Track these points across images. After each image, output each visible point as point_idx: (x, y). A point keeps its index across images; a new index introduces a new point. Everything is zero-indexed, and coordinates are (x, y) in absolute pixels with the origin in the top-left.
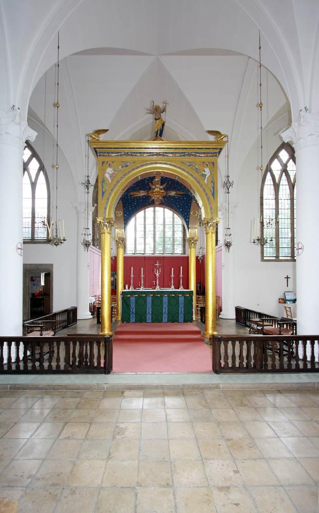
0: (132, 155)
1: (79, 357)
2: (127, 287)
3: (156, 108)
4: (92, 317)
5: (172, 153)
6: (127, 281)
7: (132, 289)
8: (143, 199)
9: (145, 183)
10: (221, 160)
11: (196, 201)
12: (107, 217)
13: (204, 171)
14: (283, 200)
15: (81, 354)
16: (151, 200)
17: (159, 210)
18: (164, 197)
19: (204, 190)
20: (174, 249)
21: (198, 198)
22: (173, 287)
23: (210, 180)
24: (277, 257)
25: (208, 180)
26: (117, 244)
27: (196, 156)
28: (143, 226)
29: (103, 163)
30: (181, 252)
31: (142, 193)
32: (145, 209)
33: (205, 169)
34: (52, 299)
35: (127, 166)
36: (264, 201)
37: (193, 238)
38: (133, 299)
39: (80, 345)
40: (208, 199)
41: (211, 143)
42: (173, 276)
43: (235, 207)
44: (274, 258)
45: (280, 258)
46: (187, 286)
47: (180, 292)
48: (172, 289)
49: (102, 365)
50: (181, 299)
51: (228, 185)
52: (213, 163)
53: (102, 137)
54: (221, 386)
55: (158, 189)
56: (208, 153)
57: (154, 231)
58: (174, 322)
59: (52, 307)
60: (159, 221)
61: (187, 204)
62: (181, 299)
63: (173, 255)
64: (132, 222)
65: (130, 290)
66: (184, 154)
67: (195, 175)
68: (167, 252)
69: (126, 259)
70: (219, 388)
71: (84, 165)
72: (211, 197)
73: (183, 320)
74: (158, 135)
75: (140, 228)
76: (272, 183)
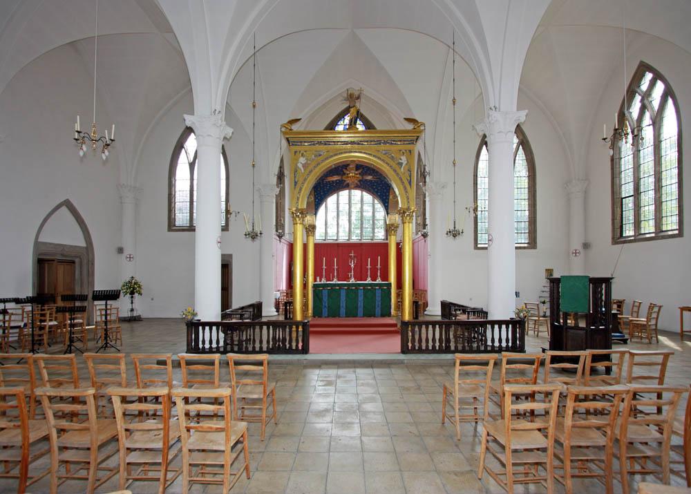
0: (326, 144)
1: (273, 341)
2: (318, 279)
4: (277, 314)
5: (367, 141)
6: (317, 273)
7: (324, 281)
8: (337, 183)
9: (340, 169)
11: (393, 189)
12: (300, 208)
13: (401, 159)
15: (274, 338)
16: (345, 183)
17: (357, 194)
18: (360, 181)
19: (401, 179)
20: (374, 233)
21: (394, 186)
22: (369, 279)
23: (407, 168)
25: (404, 169)
26: (293, 217)
27: (392, 144)
28: (336, 205)
29: (296, 152)
30: (383, 238)
31: (335, 178)
32: (338, 193)
33: (402, 158)
34: (231, 293)
35: (320, 155)
36: (479, 179)
37: (392, 225)
38: (325, 293)
39: (273, 330)
40: (405, 188)
41: (408, 132)
42: (369, 266)
43: (443, 187)
44: (526, 245)
46: (385, 276)
47: (377, 285)
48: (369, 281)
49: (300, 348)
50: (378, 293)
52: (410, 151)
53: (295, 127)
54: (406, 361)
55: (352, 174)
56: (404, 141)
57: (347, 216)
58: (370, 316)
59: (231, 302)
60: (356, 208)
61: (386, 193)
62: (378, 293)
63: (372, 242)
64: (322, 209)
65: (322, 282)
66: (379, 142)
67: (392, 163)
69: (317, 246)
70: (404, 363)
71: (273, 152)
73: (380, 314)
74: (353, 123)
75: (332, 214)
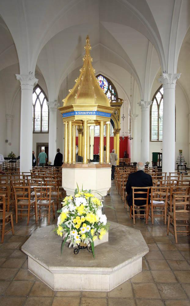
3: (116, 240)
10: (121, 108)
14: (154, 117)
24: (158, 139)
44: (40, 132)
45: (159, 140)
51: (123, 117)
52: (119, 109)
68: (97, 134)
72: (117, 120)
76: (156, 104)
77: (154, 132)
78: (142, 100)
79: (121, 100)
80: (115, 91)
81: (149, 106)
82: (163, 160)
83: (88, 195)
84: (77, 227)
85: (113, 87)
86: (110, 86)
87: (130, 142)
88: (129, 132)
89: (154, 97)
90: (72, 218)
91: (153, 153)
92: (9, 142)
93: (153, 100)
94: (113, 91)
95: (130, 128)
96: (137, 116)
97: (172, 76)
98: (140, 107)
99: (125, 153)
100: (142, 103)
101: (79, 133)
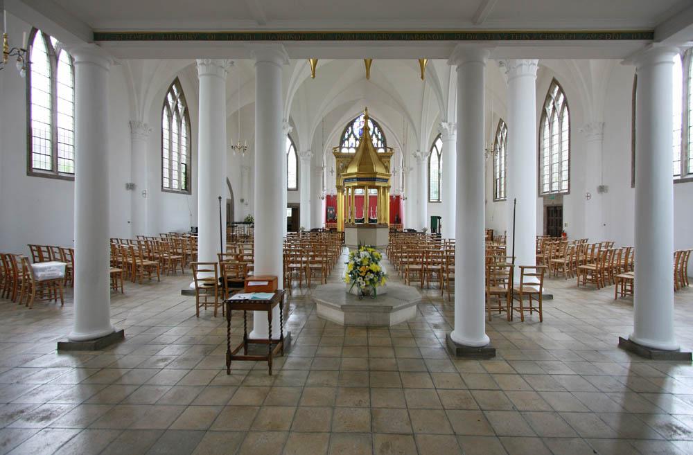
10: (392, 159)
24: (439, 200)
77: (434, 188)
78: (418, 151)
79: (391, 149)
80: (383, 135)
81: (427, 158)
82: (40, 244)
83: (371, 250)
84: (363, 274)
85: (380, 130)
86: (376, 129)
87: (403, 203)
88: (401, 189)
89: (434, 145)
90: (358, 267)
91: (432, 217)
92: (245, 202)
93: (431, 150)
94: (380, 135)
95: (403, 185)
96: (412, 169)
97: (453, 126)
98: (416, 159)
99: (396, 218)
100: (418, 154)
101: (338, 192)
